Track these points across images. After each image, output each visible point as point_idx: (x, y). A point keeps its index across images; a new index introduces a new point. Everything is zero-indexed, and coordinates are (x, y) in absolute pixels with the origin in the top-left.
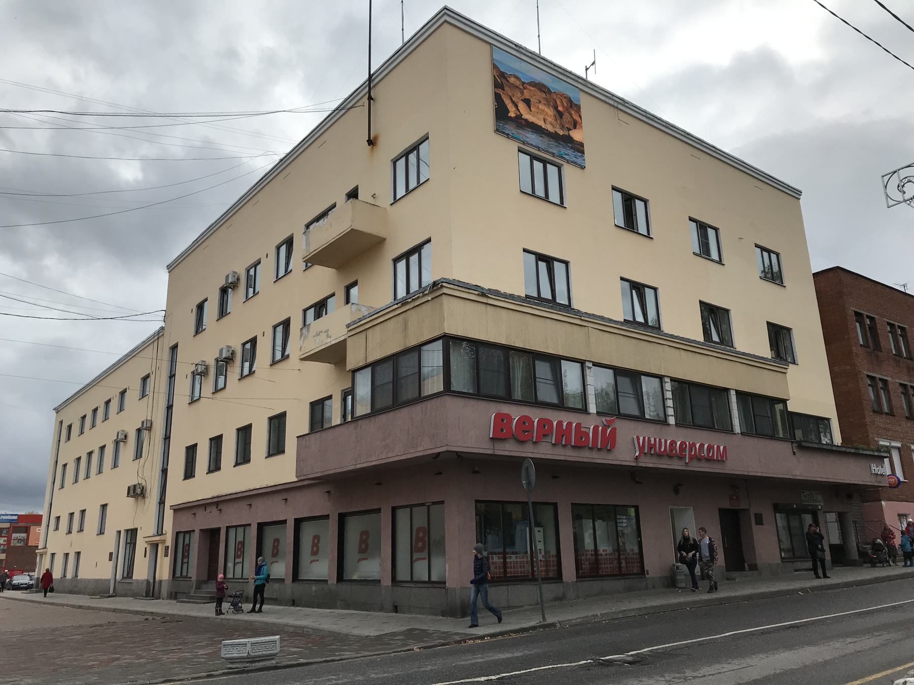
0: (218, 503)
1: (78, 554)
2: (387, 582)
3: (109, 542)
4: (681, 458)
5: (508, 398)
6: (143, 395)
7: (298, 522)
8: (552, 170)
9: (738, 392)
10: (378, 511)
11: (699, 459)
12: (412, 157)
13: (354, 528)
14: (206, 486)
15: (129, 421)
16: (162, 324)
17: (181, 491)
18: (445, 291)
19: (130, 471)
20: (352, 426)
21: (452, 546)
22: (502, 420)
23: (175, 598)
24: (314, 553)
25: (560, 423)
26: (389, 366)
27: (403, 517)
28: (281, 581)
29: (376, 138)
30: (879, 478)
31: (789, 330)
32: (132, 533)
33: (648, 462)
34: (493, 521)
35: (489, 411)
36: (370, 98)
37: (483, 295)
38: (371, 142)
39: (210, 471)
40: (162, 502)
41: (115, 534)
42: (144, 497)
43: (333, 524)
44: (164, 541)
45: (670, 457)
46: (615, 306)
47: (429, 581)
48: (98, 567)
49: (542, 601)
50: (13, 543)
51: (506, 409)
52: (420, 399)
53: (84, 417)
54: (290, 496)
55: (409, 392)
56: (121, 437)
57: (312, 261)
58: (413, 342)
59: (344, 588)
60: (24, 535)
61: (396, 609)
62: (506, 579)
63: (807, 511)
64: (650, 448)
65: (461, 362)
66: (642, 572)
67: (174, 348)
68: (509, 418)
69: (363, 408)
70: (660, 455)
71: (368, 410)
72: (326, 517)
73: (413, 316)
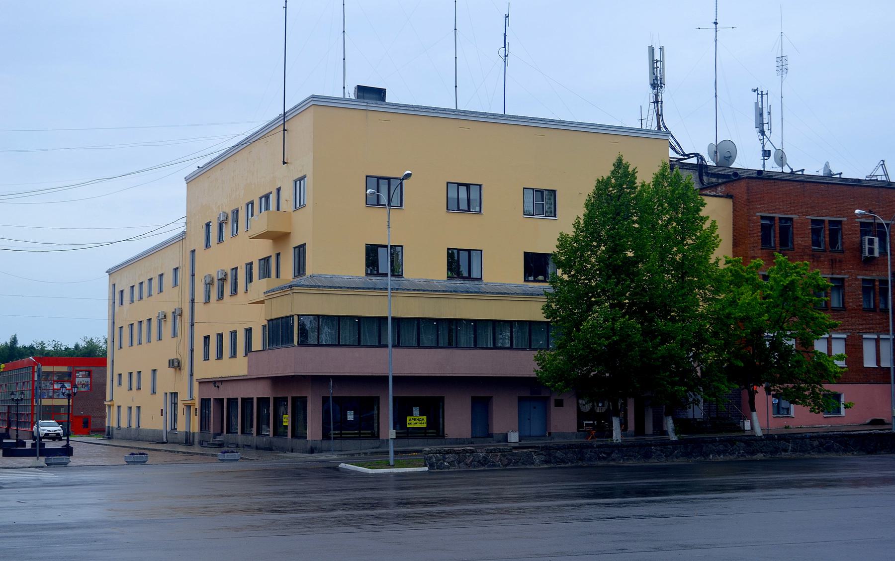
1: (139, 408)
6: (176, 285)
19: (170, 347)
32: (175, 395)
44: (194, 405)
46: (439, 272)
48: (153, 421)
53: (133, 287)
56: (161, 317)
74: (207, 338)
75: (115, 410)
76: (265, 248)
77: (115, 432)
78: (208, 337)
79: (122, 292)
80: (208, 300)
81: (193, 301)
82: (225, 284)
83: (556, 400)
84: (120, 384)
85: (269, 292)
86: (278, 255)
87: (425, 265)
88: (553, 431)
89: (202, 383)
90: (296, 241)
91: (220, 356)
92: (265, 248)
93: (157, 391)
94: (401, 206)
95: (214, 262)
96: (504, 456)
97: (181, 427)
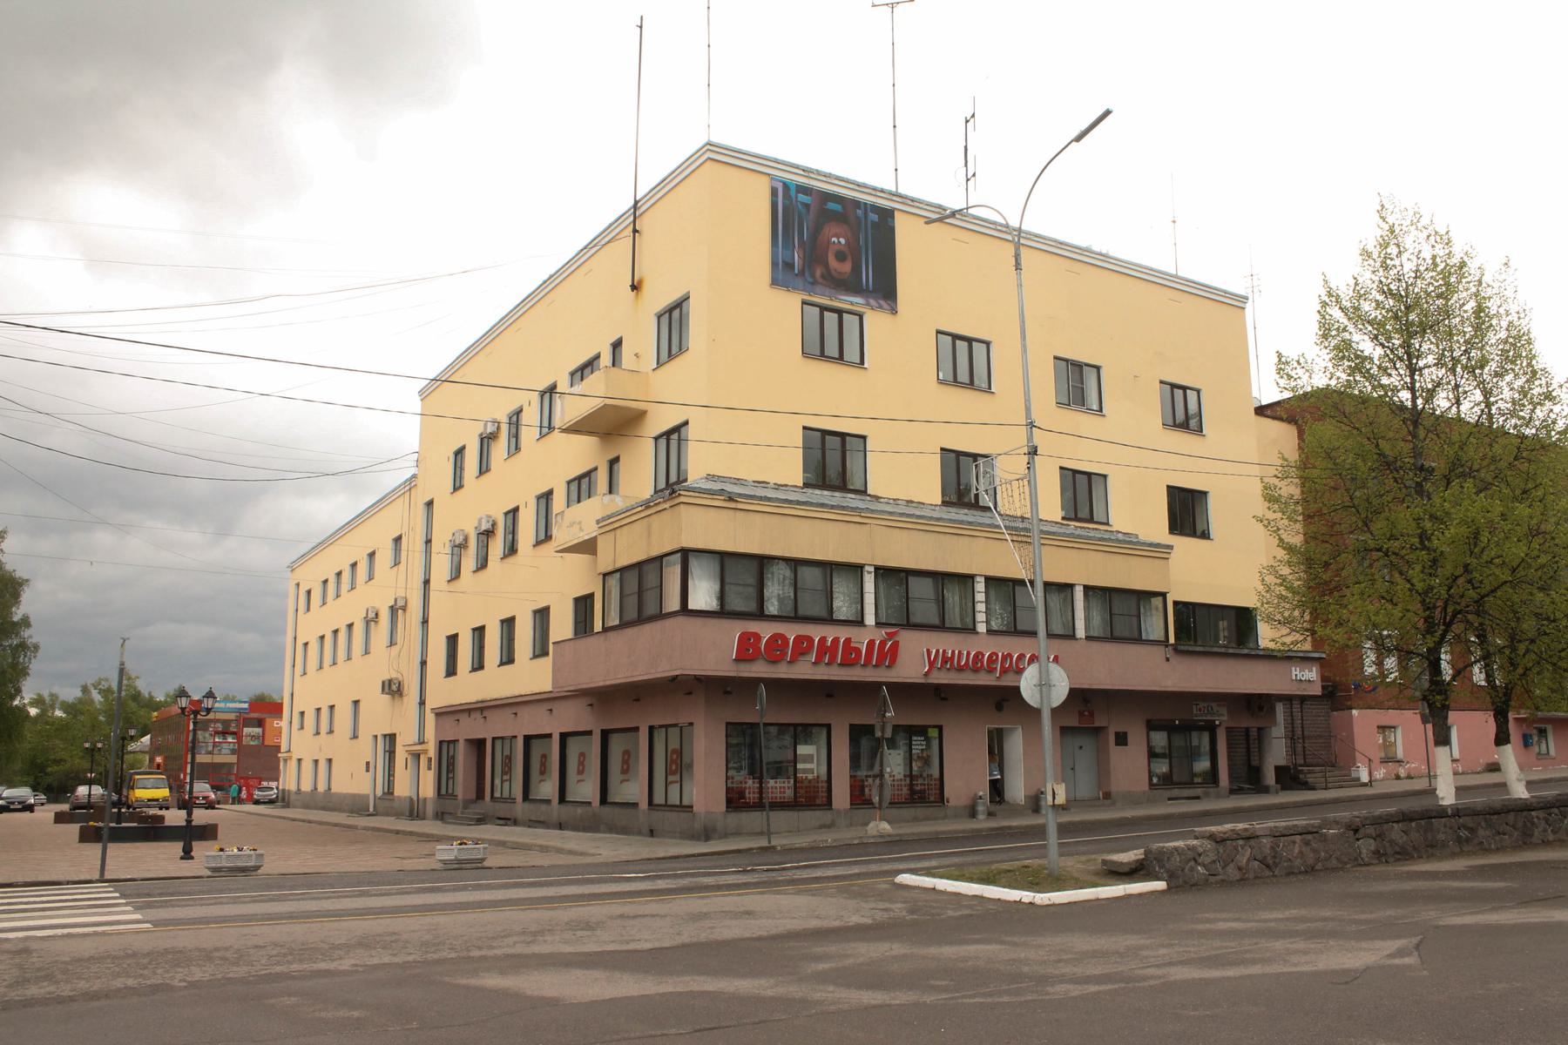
0: (482, 709)
1: (330, 761)
2: (644, 805)
3: (365, 749)
4: (991, 670)
5: (760, 615)
6: (397, 563)
7: (564, 737)
8: (850, 322)
9: (1086, 588)
10: (636, 729)
12: (676, 314)
13: (617, 746)
14: (468, 688)
15: (379, 594)
16: (413, 471)
17: (445, 692)
18: (682, 499)
19: (382, 663)
20: (602, 637)
21: (699, 769)
22: (747, 641)
23: (442, 819)
24: (580, 772)
25: (823, 640)
26: (635, 572)
27: (659, 738)
28: (548, 802)
29: (640, 282)
30: (1304, 686)
31: (1205, 493)
32: (391, 738)
34: (745, 744)
35: (733, 631)
36: (635, 231)
37: (731, 499)
38: (634, 287)
39: (474, 670)
40: (422, 703)
41: (371, 738)
42: (401, 695)
43: (596, 739)
44: (426, 751)
45: (976, 670)
46: (928, 488)
47: (666, 805)
48: (354, 779)
50: (245, 741)
51: (753, 626)
52: (661, 616)
53: (325, 582)
54: (555, 706)
55: (651, 609)
56: (371, 615)
57: (575, 429)
58: (655, 552)
60: (259, 730)
61: (652, 833)
63: (1201, 729)
64: (945, 660)
66: (941, 798)
67: (430, 504)
68: (758, 637)
69: (614, 620)
70: (960, 669)
72: (589, 733)
74: (453, 640)
75: (293, 764)
76: (580, 453)
77: (293, 798)
78: (456, 636)
79: (309, 592)
80: (456, 575)
81: (427, 582)
82: (495, 539)
83: (1117, 734)
84: (302, 728)
85: (603, 519)
86: (614, 462)
87: (902, 473)
88: (1114, 789)
89: (440, 714)
90: (661, 420)
91: (478, 665)
92: (580, 453)
93: (361, 733)
94: (862, 362)
95: (463, 514)
96: (1307, 843)
97: (403, 788)
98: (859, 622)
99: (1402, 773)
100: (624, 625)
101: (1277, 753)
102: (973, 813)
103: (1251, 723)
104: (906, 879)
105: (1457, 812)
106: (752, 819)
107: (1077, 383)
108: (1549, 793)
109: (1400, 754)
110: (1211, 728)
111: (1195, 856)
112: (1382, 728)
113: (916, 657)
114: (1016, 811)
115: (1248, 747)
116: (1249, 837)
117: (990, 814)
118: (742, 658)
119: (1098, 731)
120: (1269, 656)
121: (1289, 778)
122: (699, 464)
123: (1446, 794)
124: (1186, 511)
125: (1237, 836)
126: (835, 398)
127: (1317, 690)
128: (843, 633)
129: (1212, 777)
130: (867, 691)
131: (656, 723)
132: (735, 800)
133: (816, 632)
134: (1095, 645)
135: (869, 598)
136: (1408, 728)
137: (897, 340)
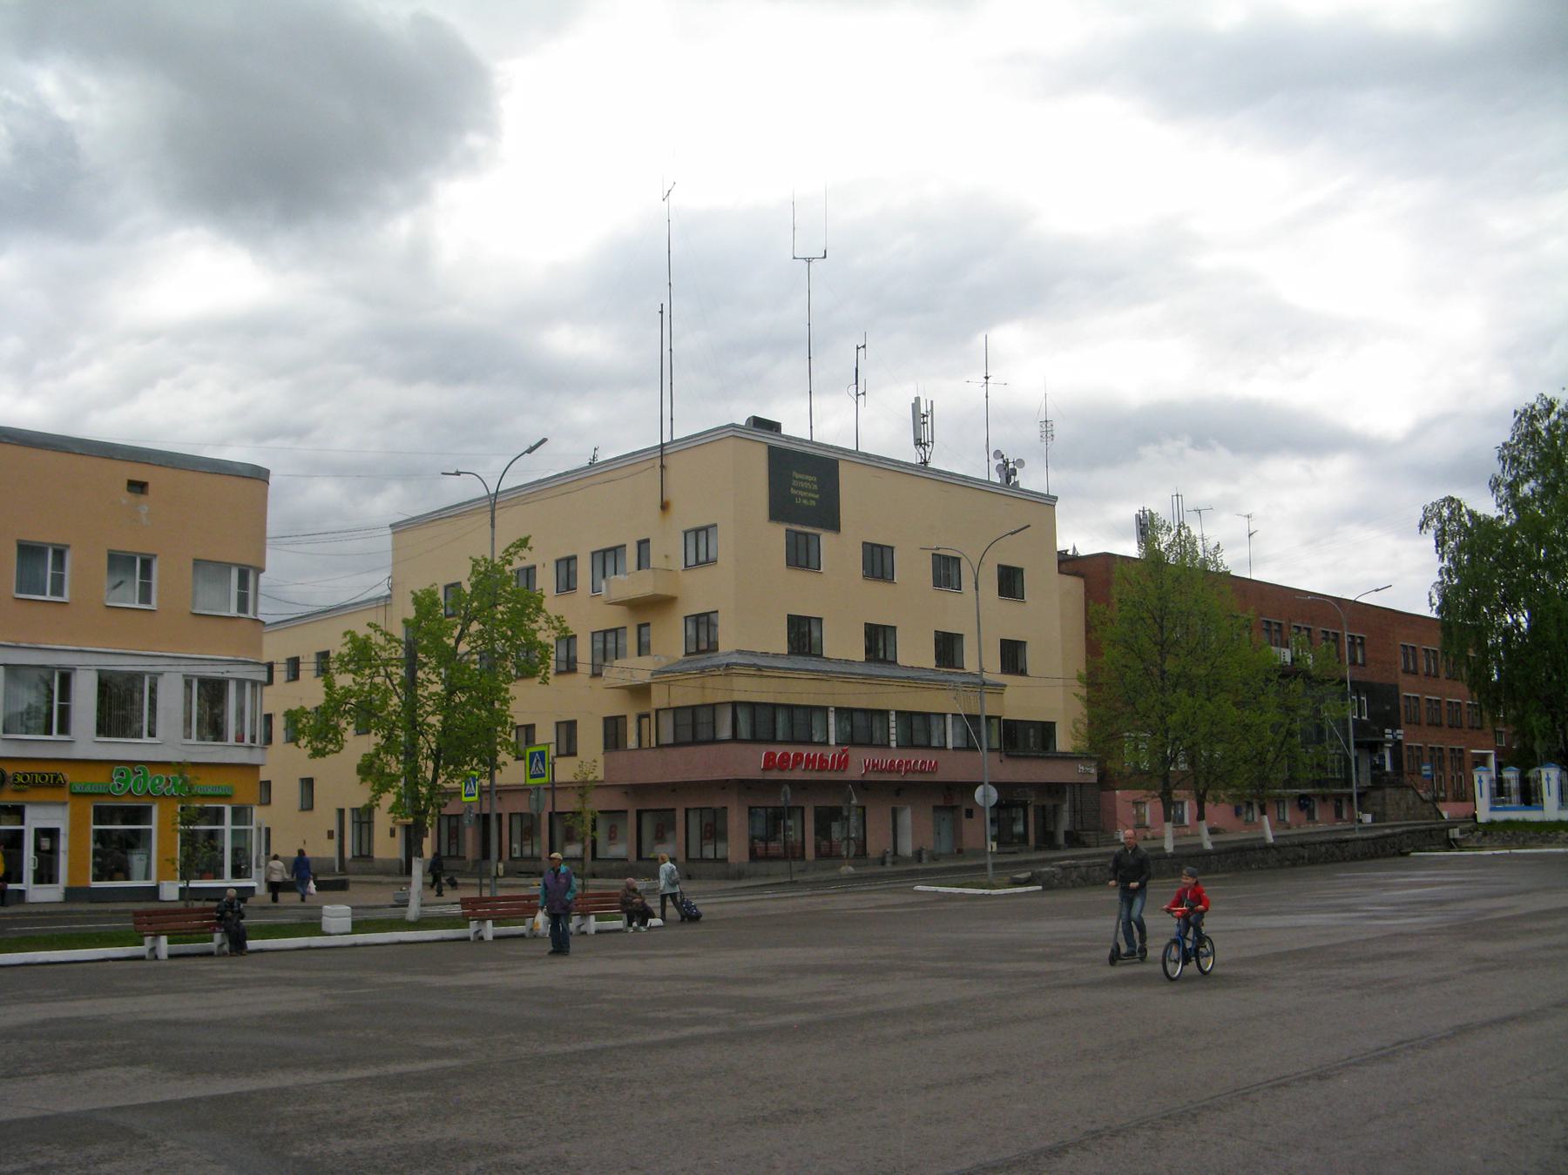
5: (773, 740)
11: (914, 772)
33: (872, 777)
35: (762, 751)
36: (662, 467)
49: (493, 512)
51: (772, 748)
52: (714, 741)
59: (642, 864)
62: (768, 857)
65: (743, 717)
70: (882, 771)
71: (671, 741)
73: (709, 682)
83: (106, 685)
85: (659, 672)
87: (843, 643)
98: (826, 743)
99: (1149, 835)
100: (677, 744)
101: (1065, 823)
102: (883, 863)
103: (1049, 803)
104: (919, 888)
105: (1173, 856)
106: (762, 866)
107: (946, 571)
108: (1223, 847)
109: (1148, 822)
110: (1025, 806)
111: (1054, 875)
112: (1136, 804)
113: (860, 763)
114: (906, 860)
115: (1046, 818)
116: (1076, 867)
117: (894, 863)
118: (767, 768)
119: (954, 808)
120: (1065, 757)
121: (1074, 839)
122: (729, 640)
123: (1169, 847)
124: (1013, 655)
125: (1071, 866)
126: (805, 594)
127: (1094, 779)
128: (818, 751)
129: (1024, 838)
130: (839, 786)
131: (691, 805)
132: (754, 856)
133: (805, 751)
134: (959, 753)
135: (832, 728)
136: (1151, 810)
137: (839, 551)
